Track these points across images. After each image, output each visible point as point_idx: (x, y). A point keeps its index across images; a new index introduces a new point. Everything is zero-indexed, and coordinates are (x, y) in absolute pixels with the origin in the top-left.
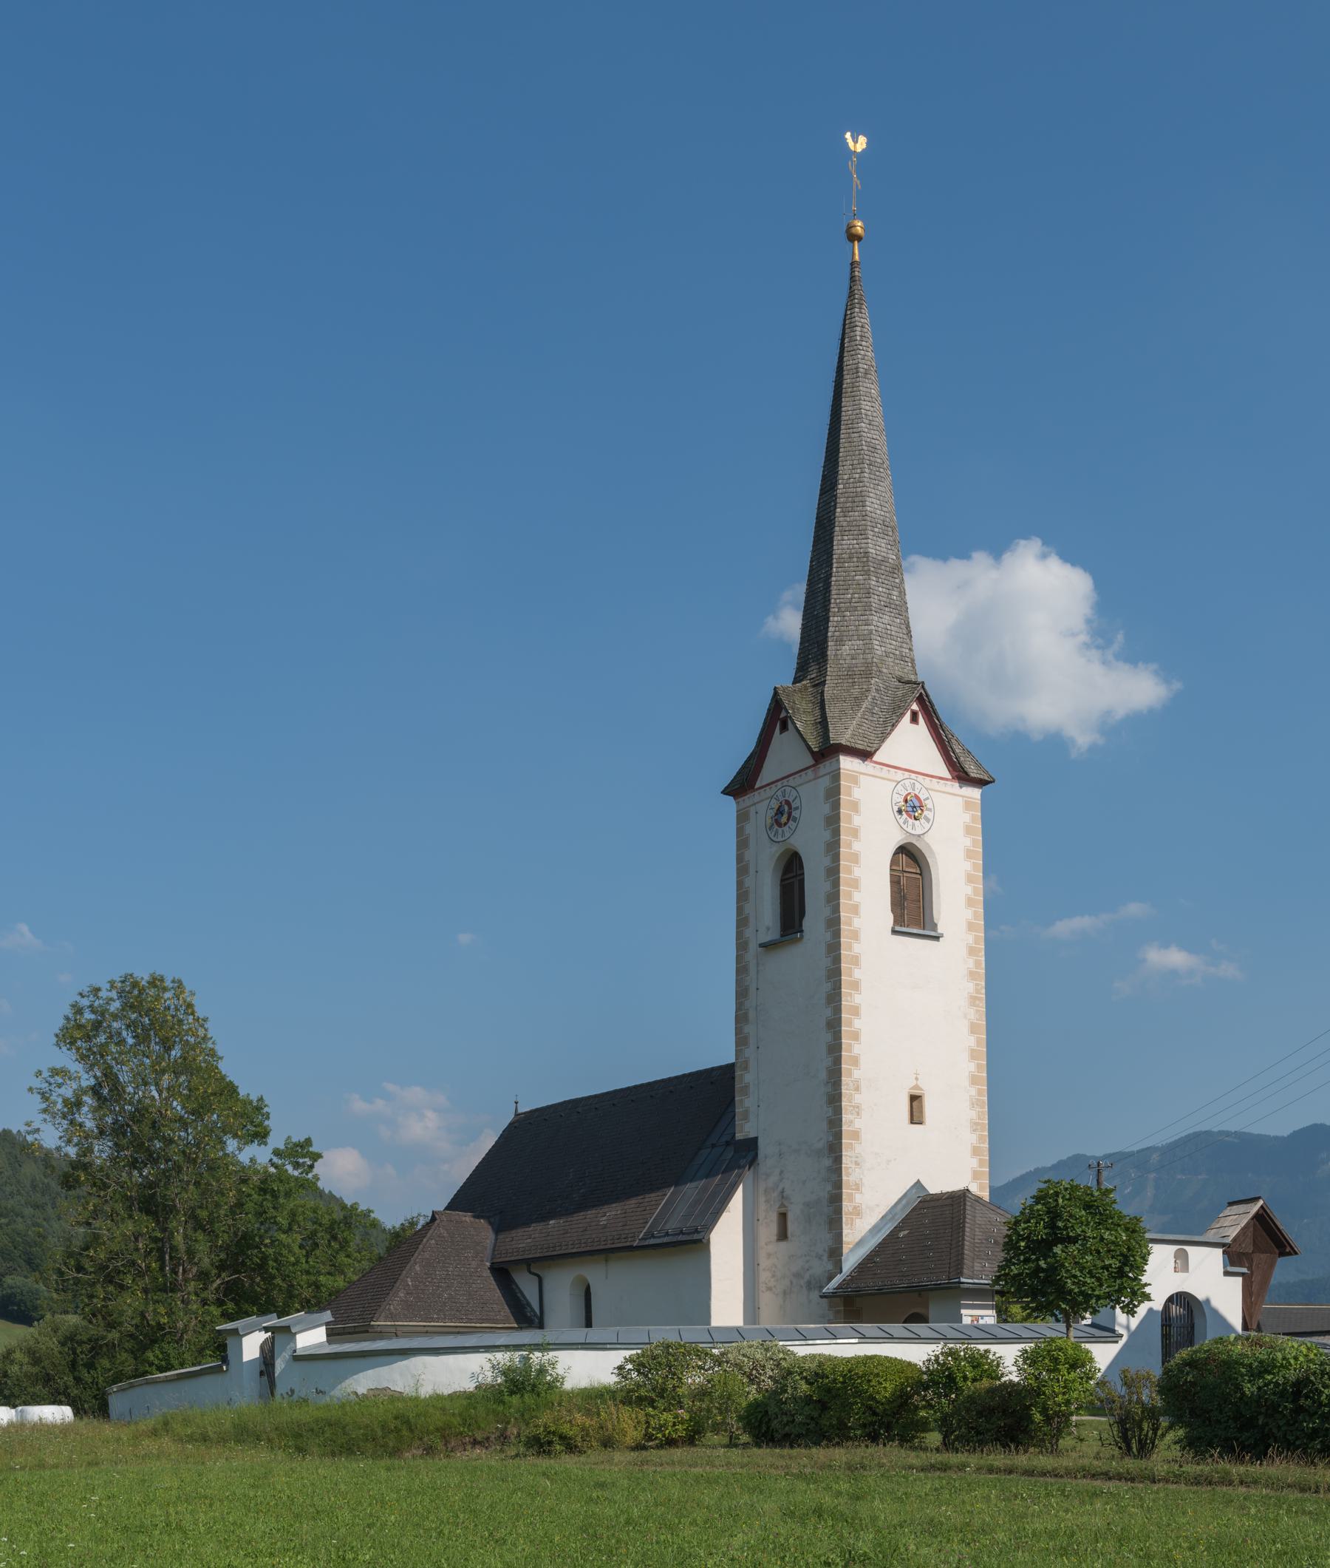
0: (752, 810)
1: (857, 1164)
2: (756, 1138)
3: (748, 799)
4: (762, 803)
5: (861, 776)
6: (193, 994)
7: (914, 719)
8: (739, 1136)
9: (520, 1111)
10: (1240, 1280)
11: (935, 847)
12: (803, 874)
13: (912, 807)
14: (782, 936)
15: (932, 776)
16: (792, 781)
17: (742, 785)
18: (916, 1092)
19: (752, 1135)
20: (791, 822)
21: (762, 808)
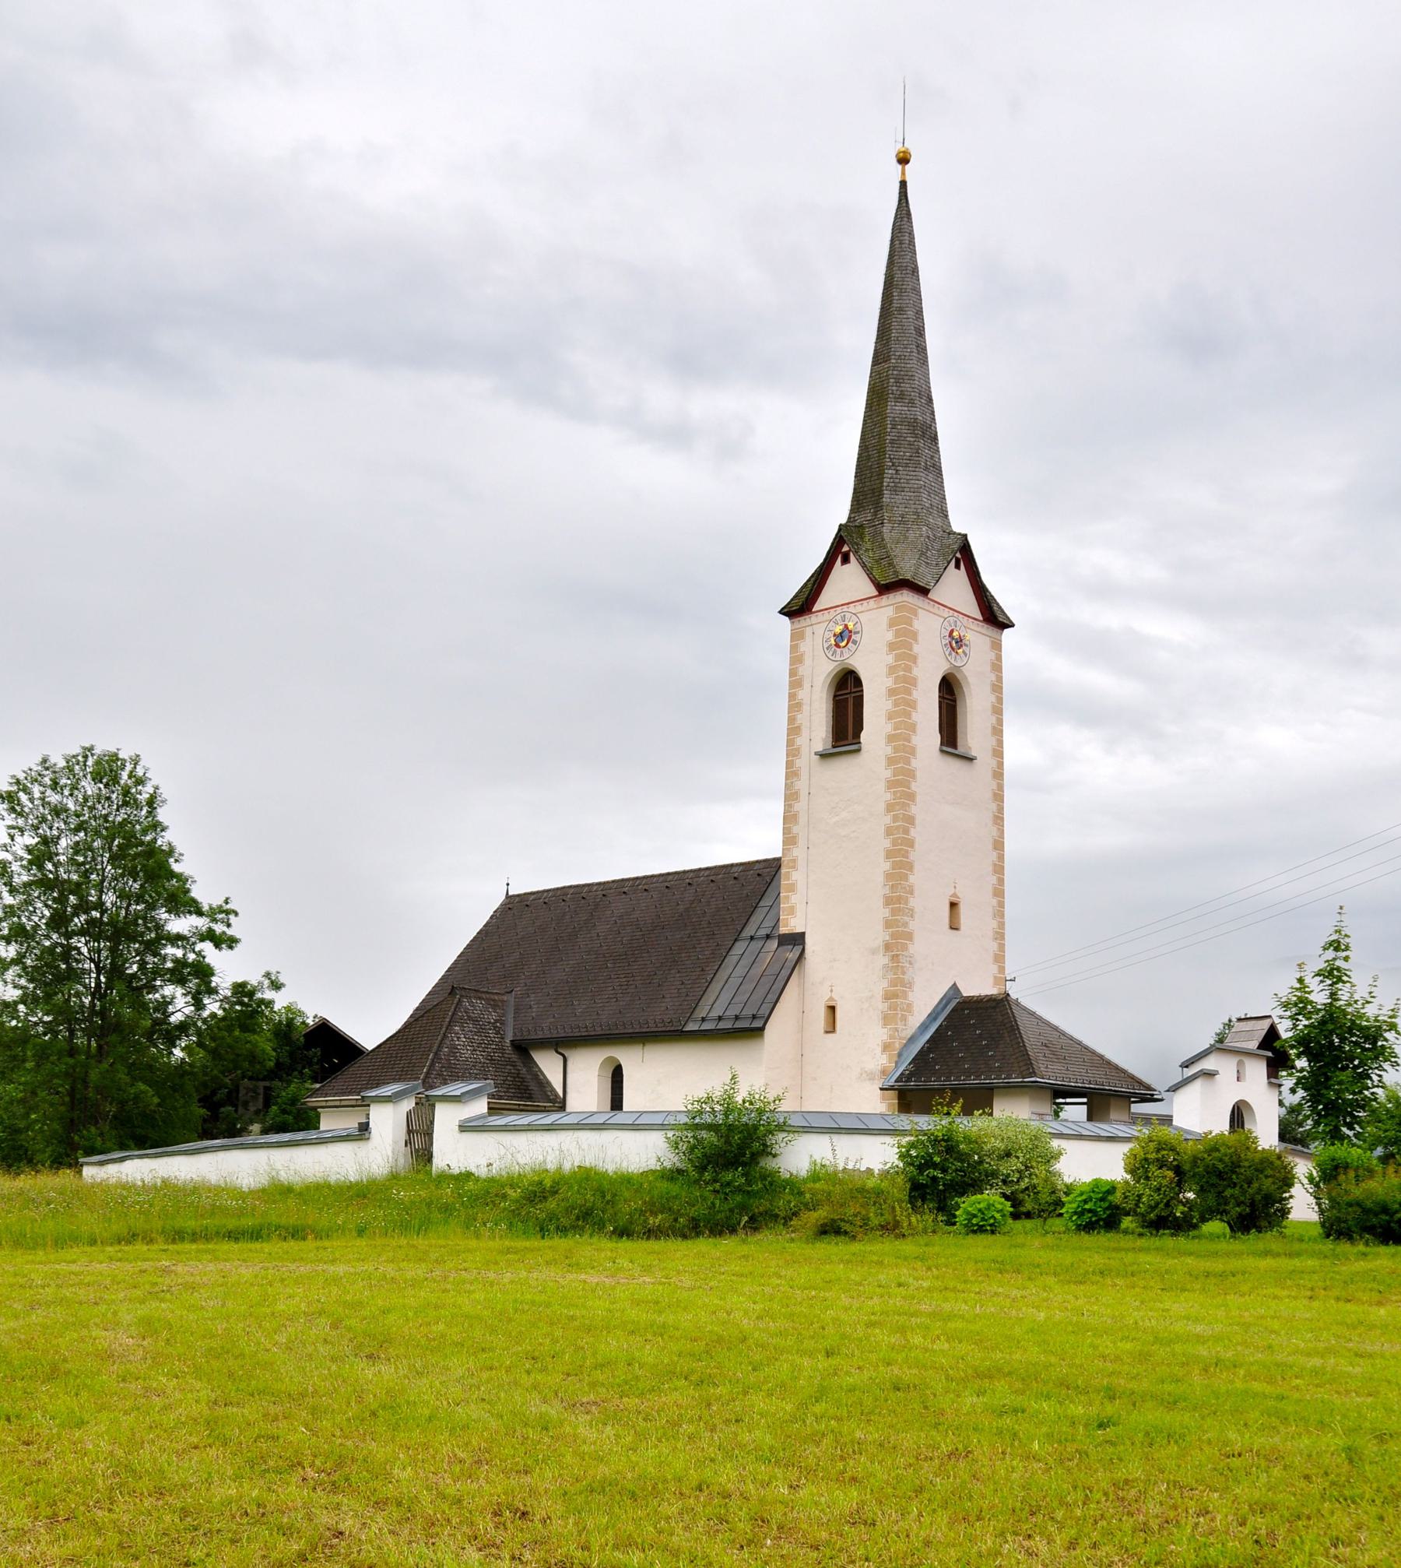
0: (808, 631)
1: (910, 963)
2: (803, 934)
3: (804, 621)
4: (819, 626)
5: (920, 610)
6: (136, 761)
7: (957, 566)
8: (783, 930)
9: (510, 893)
10: (1085, 1106)
11: (971, 679)
12: (862, 691)
13: (956, 643)
14: (834, 747)
15: (968, 617)
16: (851, 608)
17: (800, 607)
18: (954, 899)
19: (799, 930)
20: (850, 644)
21: (820, 630)
